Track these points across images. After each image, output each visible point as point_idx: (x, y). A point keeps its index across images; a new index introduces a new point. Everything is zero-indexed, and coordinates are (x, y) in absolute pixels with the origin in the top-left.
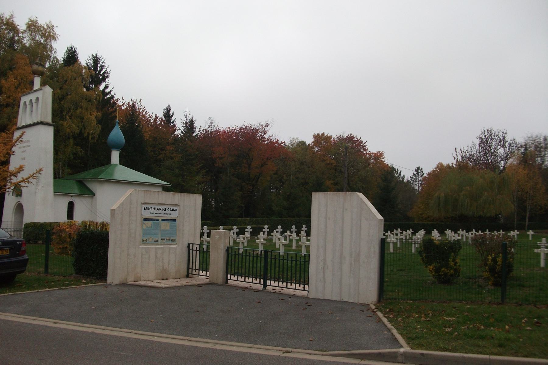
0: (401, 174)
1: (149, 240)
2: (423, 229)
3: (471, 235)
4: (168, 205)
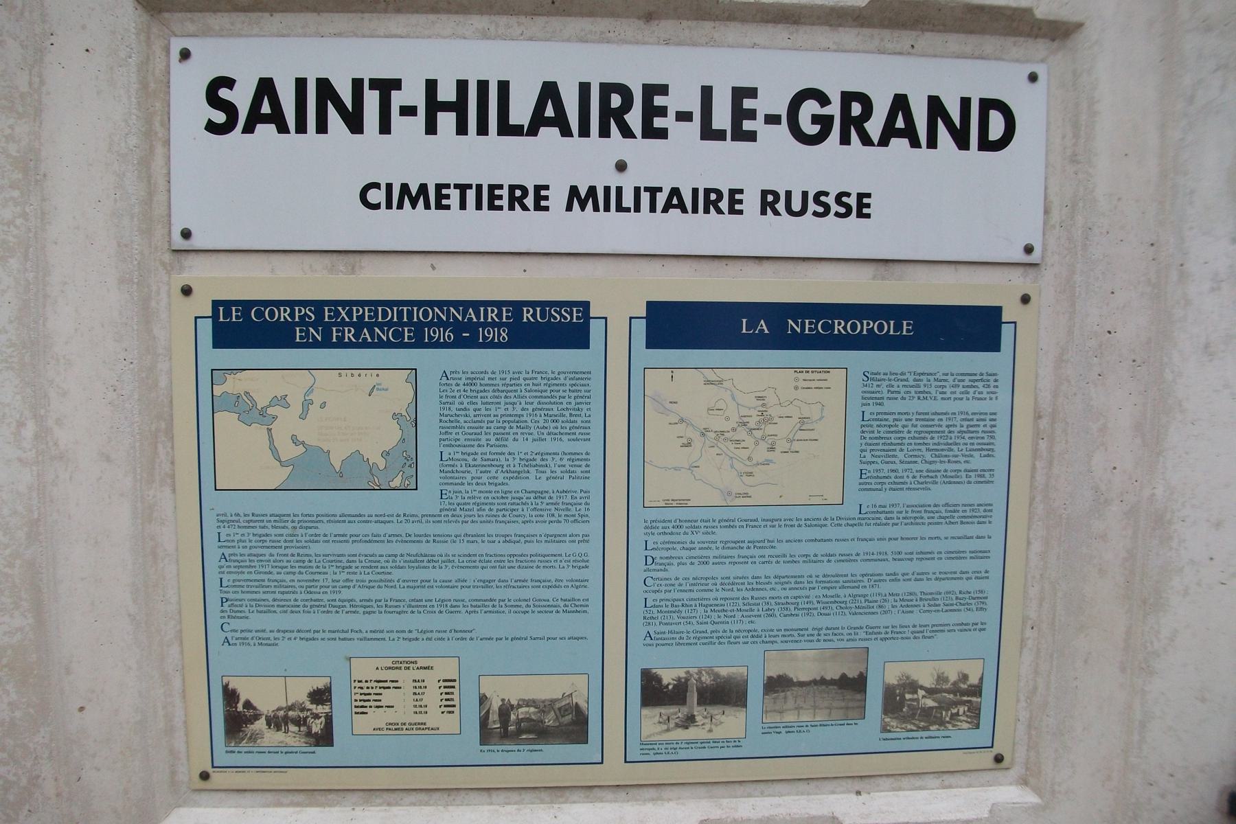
0: (844, 676)
1: (365, 702)
4: (805, 35)
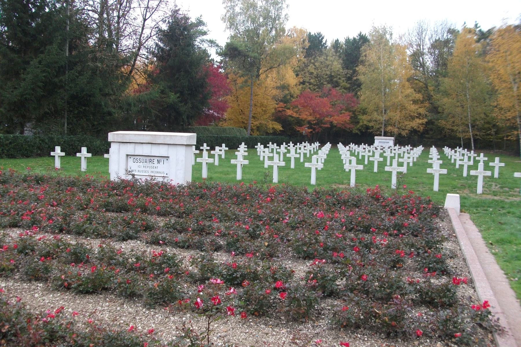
2: (329, 143)
3: (218, 151)
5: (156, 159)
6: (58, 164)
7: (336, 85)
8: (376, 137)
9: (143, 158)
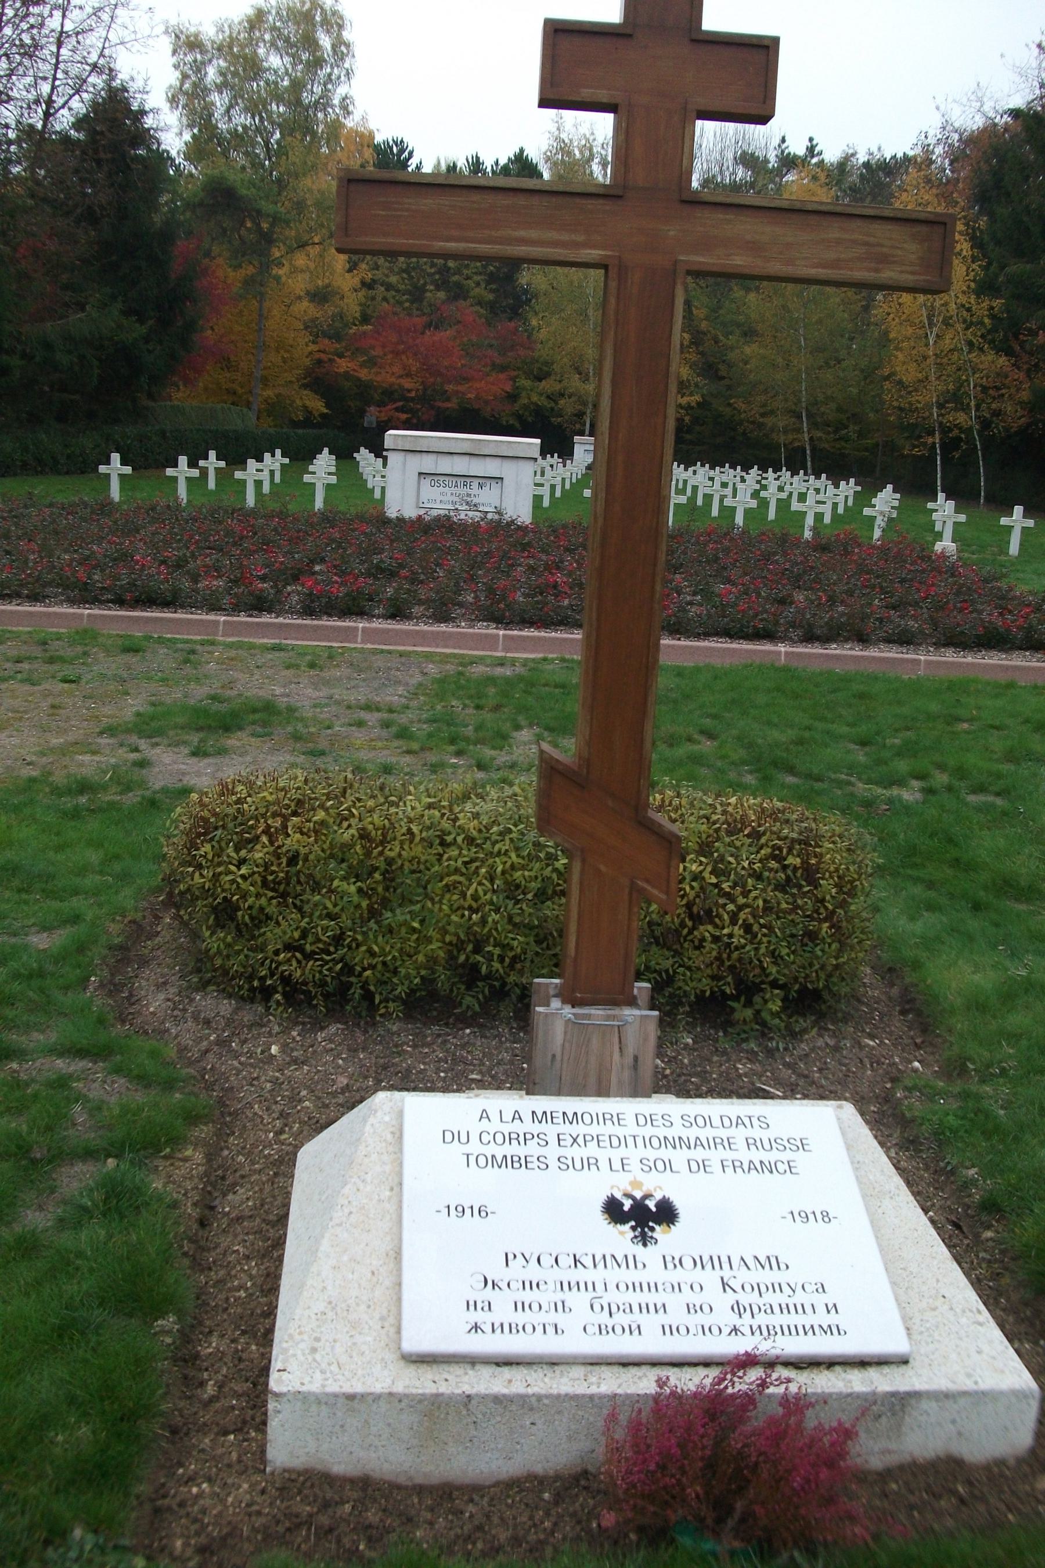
5: (475, 483)
6: (115, 492)
7: (459, 293)
8: (576, 438)
9: (451, 478)
